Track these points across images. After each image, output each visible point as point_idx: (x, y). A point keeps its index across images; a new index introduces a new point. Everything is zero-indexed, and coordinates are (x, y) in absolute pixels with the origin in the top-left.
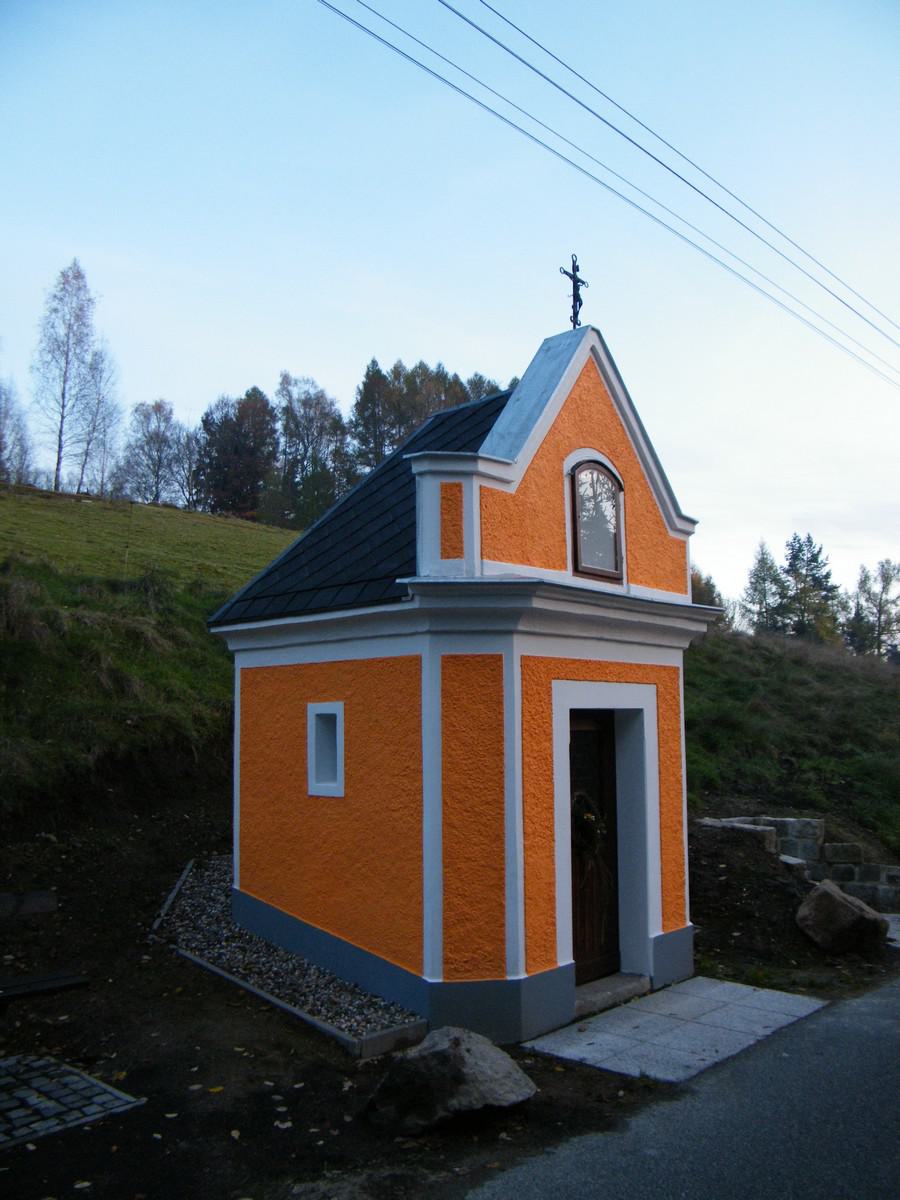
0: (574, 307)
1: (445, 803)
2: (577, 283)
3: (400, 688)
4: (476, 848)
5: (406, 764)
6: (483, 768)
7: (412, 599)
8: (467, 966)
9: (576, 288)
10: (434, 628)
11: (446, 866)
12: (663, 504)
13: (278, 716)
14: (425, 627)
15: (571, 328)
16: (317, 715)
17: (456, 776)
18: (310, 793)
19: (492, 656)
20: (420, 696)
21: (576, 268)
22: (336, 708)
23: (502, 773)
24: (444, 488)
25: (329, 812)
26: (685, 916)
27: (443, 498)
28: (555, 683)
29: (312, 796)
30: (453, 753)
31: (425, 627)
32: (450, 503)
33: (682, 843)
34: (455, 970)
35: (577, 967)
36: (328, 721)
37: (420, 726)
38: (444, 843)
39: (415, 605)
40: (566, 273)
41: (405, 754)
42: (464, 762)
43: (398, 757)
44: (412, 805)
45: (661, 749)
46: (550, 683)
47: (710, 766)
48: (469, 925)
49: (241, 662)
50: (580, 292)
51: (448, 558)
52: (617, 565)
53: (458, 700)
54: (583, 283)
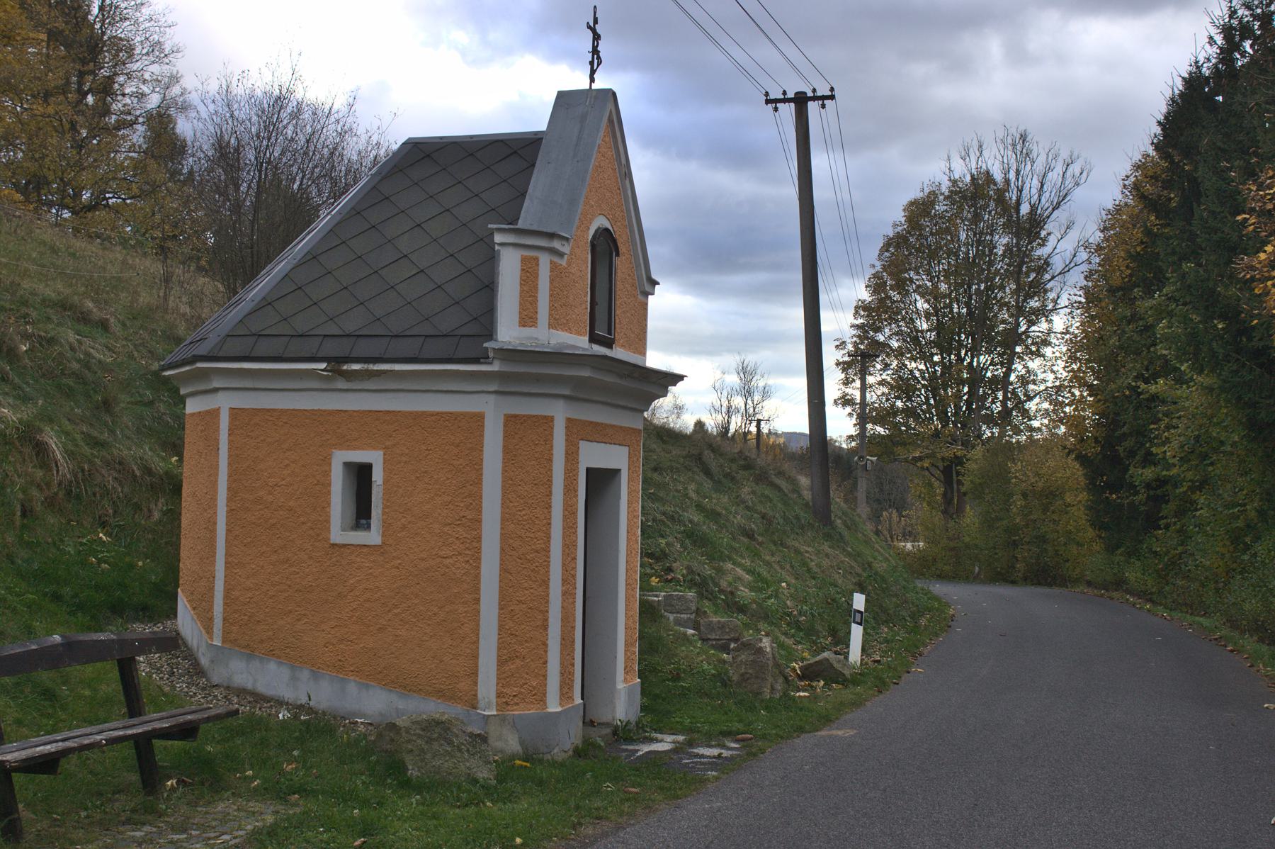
1: (502, 550)
2: (596, 37)
4: (527, 592)
5: (462, 514)
6: (533, 518)
10: (501, 389)
11: (501, 608)
16: (344, 463)
18: (332, 542)
19: (545, 417)
20: (482, 451)
22: (374, 457)
23: (549, 524)
24: (524, 260)
25: (358, 560)
27: (523, 270)
29: (334, 545)
34: (507, 703)
36: (361, 475)
37: (481, 480)
38: (500, 587)
39: (495, 367)
41: (462, 505)
42: (519, 513)
43: (452, 507)
44: (467, 552)
47: (503, 532)
51: (524, 326)
53: (515, 456)
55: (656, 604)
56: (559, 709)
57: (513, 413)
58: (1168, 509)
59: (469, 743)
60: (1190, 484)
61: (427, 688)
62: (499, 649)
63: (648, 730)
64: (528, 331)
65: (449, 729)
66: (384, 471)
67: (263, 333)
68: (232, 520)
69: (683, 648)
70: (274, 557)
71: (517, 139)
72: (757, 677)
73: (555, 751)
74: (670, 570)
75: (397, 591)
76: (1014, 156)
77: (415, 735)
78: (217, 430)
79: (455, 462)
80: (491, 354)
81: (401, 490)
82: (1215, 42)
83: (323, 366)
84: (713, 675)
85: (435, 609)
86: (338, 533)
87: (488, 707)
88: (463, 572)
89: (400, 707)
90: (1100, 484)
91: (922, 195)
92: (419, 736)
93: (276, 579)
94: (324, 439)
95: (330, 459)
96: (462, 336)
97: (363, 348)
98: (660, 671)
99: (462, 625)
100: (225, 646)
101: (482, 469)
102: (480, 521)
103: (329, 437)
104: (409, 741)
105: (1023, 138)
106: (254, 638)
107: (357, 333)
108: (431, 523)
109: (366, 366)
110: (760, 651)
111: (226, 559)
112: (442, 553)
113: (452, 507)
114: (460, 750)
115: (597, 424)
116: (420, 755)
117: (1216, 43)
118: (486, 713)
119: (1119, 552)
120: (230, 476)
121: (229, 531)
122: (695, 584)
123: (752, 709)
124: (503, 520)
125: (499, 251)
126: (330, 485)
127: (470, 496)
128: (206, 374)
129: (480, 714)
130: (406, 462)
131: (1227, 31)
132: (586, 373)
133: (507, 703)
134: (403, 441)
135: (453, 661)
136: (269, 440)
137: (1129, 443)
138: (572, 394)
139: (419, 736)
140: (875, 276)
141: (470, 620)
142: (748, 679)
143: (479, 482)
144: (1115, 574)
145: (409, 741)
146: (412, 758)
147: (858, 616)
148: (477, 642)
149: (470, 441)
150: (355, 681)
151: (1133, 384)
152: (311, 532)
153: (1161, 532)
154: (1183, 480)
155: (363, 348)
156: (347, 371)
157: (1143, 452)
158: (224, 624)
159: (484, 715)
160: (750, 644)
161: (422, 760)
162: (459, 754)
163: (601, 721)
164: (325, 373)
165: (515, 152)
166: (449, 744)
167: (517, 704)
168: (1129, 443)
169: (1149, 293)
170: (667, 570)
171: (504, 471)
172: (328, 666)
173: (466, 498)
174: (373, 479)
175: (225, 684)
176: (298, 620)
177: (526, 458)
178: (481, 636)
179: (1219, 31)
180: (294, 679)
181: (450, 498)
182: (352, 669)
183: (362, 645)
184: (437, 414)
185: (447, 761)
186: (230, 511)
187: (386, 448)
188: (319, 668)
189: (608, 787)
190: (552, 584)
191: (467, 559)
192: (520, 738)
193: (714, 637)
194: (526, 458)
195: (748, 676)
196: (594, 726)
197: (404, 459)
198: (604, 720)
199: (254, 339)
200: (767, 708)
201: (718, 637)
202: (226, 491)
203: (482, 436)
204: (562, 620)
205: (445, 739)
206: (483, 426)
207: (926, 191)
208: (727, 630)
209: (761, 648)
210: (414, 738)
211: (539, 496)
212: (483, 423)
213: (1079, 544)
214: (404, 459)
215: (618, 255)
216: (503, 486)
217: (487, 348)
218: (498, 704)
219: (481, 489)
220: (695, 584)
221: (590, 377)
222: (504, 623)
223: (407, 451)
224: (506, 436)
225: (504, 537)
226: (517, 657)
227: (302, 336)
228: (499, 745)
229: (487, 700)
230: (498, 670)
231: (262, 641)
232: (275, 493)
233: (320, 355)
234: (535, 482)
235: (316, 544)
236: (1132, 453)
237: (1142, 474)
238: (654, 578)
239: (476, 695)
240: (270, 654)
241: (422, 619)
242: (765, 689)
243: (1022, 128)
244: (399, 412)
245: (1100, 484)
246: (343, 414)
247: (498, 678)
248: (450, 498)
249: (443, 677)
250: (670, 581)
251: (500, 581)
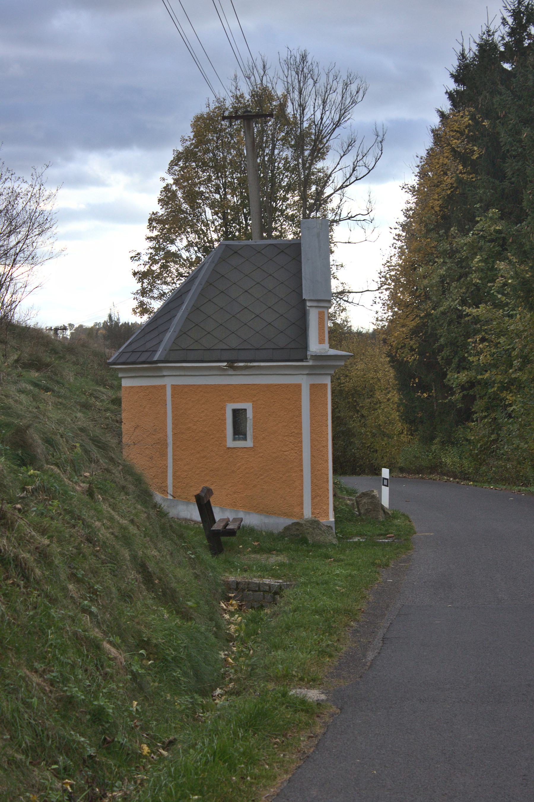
1: (311, 447)
5: (292, 431)
10: (311, 373)
11: (312, 474)
22: (248, 406)
29: (229, 448)
37: (301, 415)
39: (310, 363)
44: (296, 448)
58: (479, 404)
60: (499, 385)
64: (322, 346)
70: (198, 455)
72: (374, 510)
76: (297, 76)
78: (165, 395)
82: (507, 22)
83: (225, 364)
86: (230, 443)
90: (413, 386)
91: (207, 110)
102: (301, 434)
104: (307, 529)
105: (304, 58)
107: (238, 348)
109: (246, 364)
111: (173, 457)
112: (283, 449)
114: (325, 533)
117: (508, 24)
119: (435, 441)
120: (173, 417)
124: (311, 433)
125: (309, 310)
126: (225, 420)
127: (296, 422)
128: (160, 369)
131: (516, 14)
135: (291, 499)
137: (446, 353)
139: (310, 527)
140: (167, 189)
142: (370, 511)
143: (300, 416)
144: (430, 460)
147: (385, 482)
150: (243, 511)
151: (460, 308)
152: (217, 442)
153: (473, 423)
154: (494, 382)
156: (236, 366)
157: (457, 359)
165: (282, 251)
168: (446, 353)
169: (464, 232)
171: (311, 410)
174: (248, 416)
179: (510, 14)
184: (278, 385)
186: (174, 434)
187: (253, 401)
202: (171, 424)
203: (301, 394)
205: (319, 528)
206: (301, 390)
207: (212, 107)
209: (374, 495)
213: (390, 437)
216: (310, 417)
223: (264, 403)
224: (311, 394)
227: (209, 349)
233: (223, 359)
236: (449, 362)
237: (457, 378)
239: (303, 514)
243: (302, 49)
245: (413, 386)
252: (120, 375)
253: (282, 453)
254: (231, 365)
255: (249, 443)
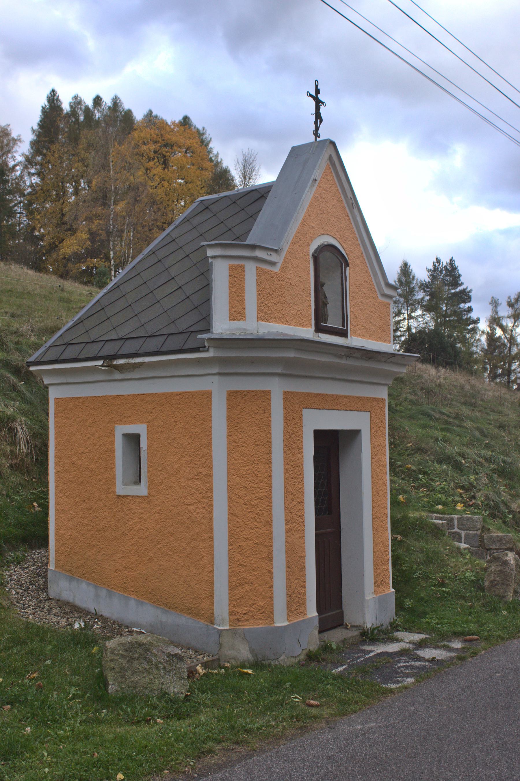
0: (316, 123)
1: (230, 498)
2: (318, 103)
3: (193, 414)
4: (252, 531)
7: (208, 351)
8: (246, 617)
9: (318, 108)
10: (221, 371)
11: (230, 545)
12: (375, 275)
13: (89, 435)
14: (215, 370)
15: (313, 140)
16: (123, 434)
17: (238, 478)
18: (117, 494)
19: (263, 392)
20: (211, 421)
21: (318, 91)
24: (232, 268)
25: (134, 507)
26: (389, 584)
28: (305, 411)
29: (119, 496)
30: (236, 462)
31: (215, 370)
32: (235, 279)
33: (387, 529)
34: (238, 620)
35: (320, 619)
37: (211, 443)
38: (229, 527)
39: (211, 354)
40: (311, 96)
44: (204, 500)
45: (374, 460)
46: (301, 411)
47: (230, 483)
48: (247, 587)
49: (53, 394)
50: (320, 111)
51: (234, 320)
52: (344, 319)
53: (238, 423)
54: (323, 103)
55: (440, 526)
56: (286, 623)
57: (235, 389)
59: (166, 662)
61: (181, 606)
62: (230, 577)
63: (401, 629)
65: (149, 650)
66: (148, 439)
67: (70, 343)
68: (58, 479)
69: (454, 560)
71: (266, 187)
72: (503, 584)
73: (282, 658)
74: (474, 497)
75: (159, 530)
77: (118, 655)
79: (193, 430)
80: (206, 344)
81: (159, 454)
83: (100, 363)
84: (472, 581)
85: (184, 545)
86: (121, 489)
87: (222, 623)
88: (201, 516)
89: (164, 620)
92: (122, 656)
93: (85, 521)
94: (110, 417)
95: (114, 432)
96: (192, 332)
97: (129, 347)
98: (431, 578)
99: (203, 557)
100: (56, 570)
101: (211, 434)
102: (211, 476)
103: (113, 416)
104: (112, 660)
106: (74, 565)
107: (125, 337)
108: (179, 479)
110: (506, 563)
111: (56, 507)
112: (187, 501)
113: (193, 466)
114: (157, 668)
115: (325, 395)
116: (120, 672)
118: (220, 628)
121: (56, 486)
122: (490, 507)
123: (495, 610)
125: (212, 262)
126: (114, 451)
129: (217, 629)
130: (161, 432)
132: (291, 354)
133: (238, 620)
134: (159, 416)
135: (198, 586)
136: (78, 420)
138: (284, 372)
139: (122, 656)
141: (208, 554)
142: (496, 585)
143: (209, 445)
145: (112, 660)
146: (113, 674)
148: (212, 571)
149: (203, 413)
150: (134, 599)
152: (105, 486)
155: (129, 347)
158: (56, 554)
159: (219, 630)
160: (499, 558)
161: (122, 677)
162: (156, 672)
163: (355, 624)
164: (103, 368)
166: (148, 662)
167: (247, 620)
170: (471, 498)
171: (229, 435)
172: (118, 587)
173: (201, 458)
175: (57, 598)
176: (99, 552)
177: (248, 424)
178: (215, 566)
180: (97, 596)
181: (191, 458)
182: (133, 590)
183: (138, 572)
184: (180, 394)
185: (145, 677)
188: (112, 588)
189: (296, 698)
190: (275, 524)
191: (204, 506)
192: (250, 648)
193: (494, 547)
194: (248, 424)
195: (496, 582)
196: (348, 629)
197: (160, 430)
198: (357, 623)
199: (64, 347)
200: (508, 609)
201: (497, 547)
203: (210, 409)
204: (286, 552)
206: (210, 401)
208: (504, 542)
209: (506, 560)
210: (117, 658)
211: (261, 454)
212: (211, 399)
214: (160, 430)
215: (347, 265)
217: (203, 339)
218: (230, 621)
219: (211, 450)
220: (490, 507)
221: (294, 357)
222: (233, 556)
223: (162, 423)
225: (231, 488)
226: (246, 582)
228: (232, 653)
229: (221, 617)
230: (230, 593)
231: (78, 567)
232: (83, 458)
234: (256, 443)
235: (108, 495)
238: (459, 504)
239: (213, 613)
240: (83, 576)
241: (176, 553)
242: (509, 593)
244: (156, 394)
246: (122, 398)
247: (229, 600)
248: (191, 458)
249: (191, 598)
250: (472, 506)
251: (229, 523)
252: (46, 382)
253: (185, 507)
254: (110, 363)
255: (142, 490)
